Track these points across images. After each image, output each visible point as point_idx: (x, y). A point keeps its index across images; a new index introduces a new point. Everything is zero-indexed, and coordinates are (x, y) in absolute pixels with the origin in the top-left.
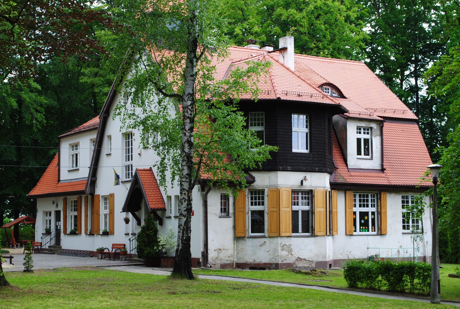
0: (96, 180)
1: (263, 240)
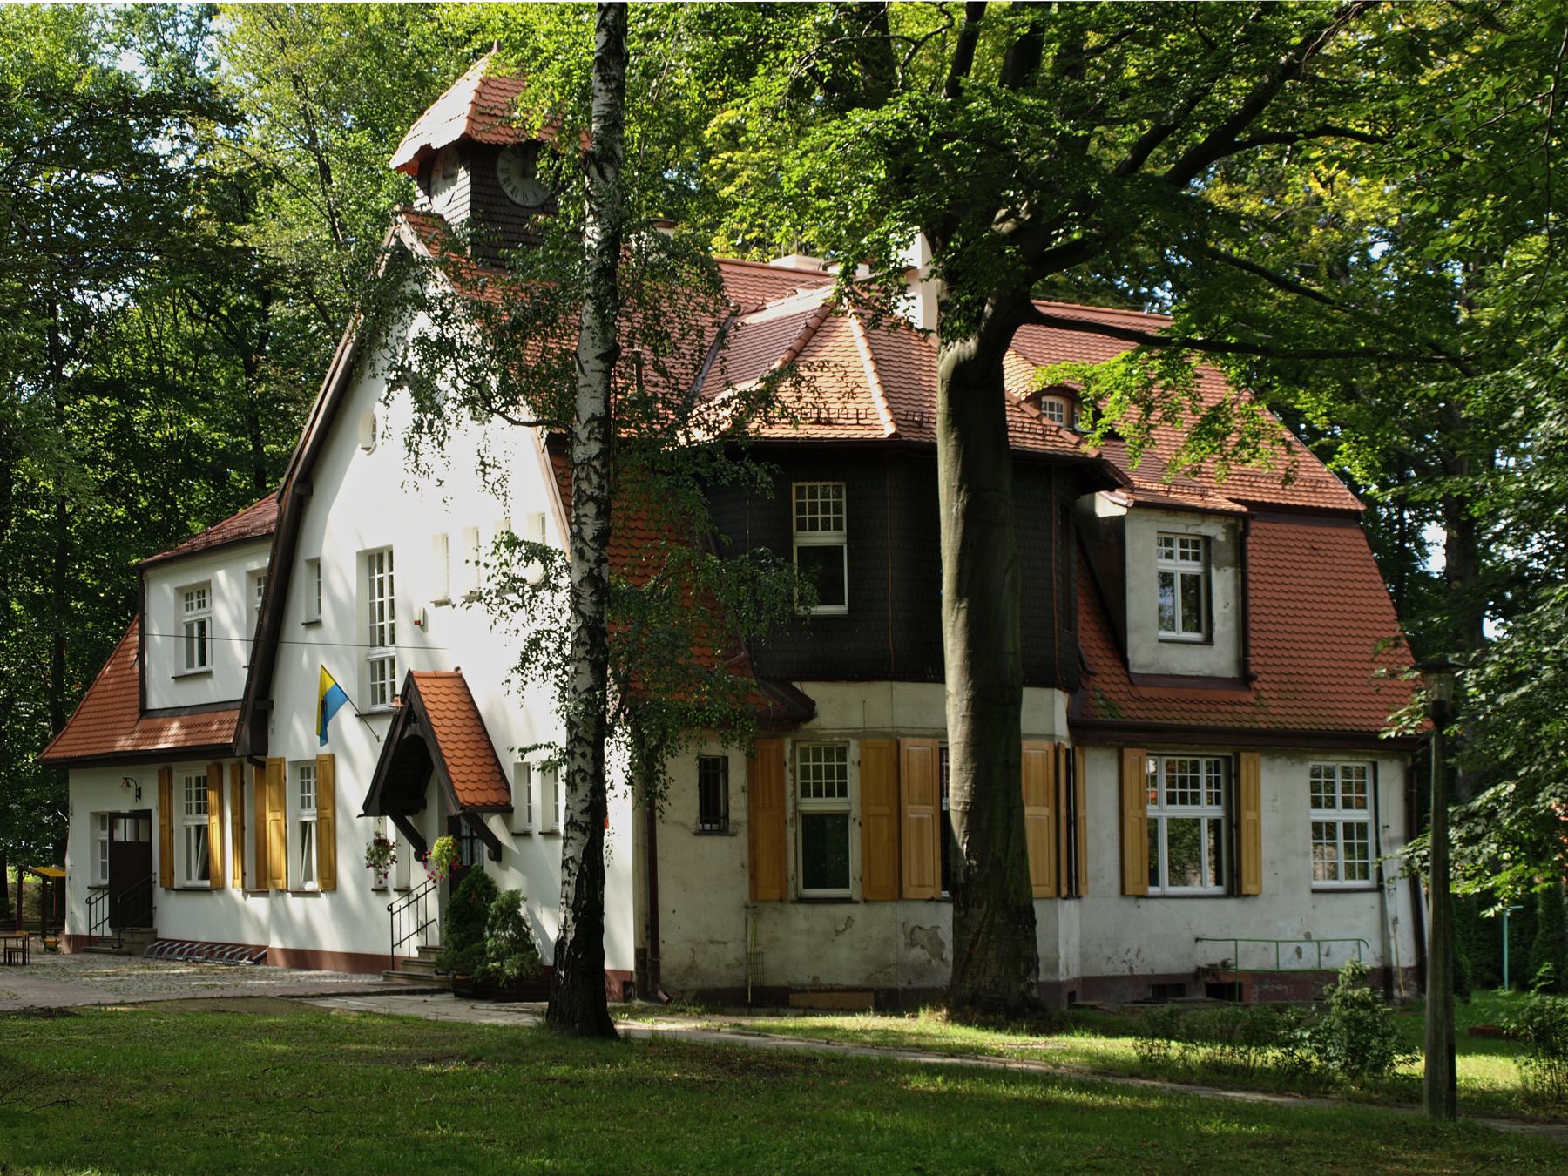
0: (272, 707)
1: (843, 910)
